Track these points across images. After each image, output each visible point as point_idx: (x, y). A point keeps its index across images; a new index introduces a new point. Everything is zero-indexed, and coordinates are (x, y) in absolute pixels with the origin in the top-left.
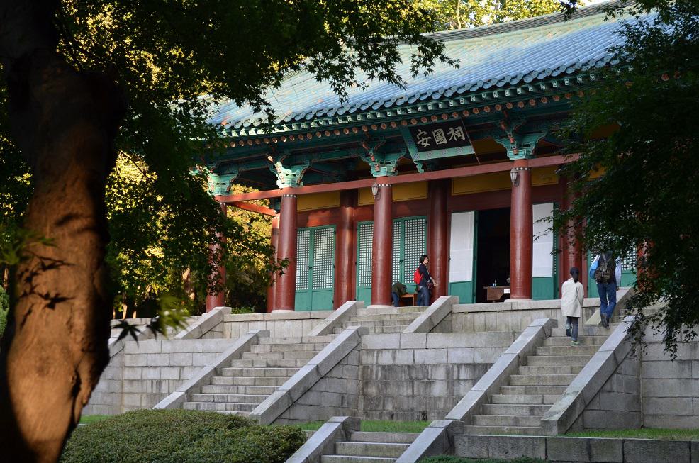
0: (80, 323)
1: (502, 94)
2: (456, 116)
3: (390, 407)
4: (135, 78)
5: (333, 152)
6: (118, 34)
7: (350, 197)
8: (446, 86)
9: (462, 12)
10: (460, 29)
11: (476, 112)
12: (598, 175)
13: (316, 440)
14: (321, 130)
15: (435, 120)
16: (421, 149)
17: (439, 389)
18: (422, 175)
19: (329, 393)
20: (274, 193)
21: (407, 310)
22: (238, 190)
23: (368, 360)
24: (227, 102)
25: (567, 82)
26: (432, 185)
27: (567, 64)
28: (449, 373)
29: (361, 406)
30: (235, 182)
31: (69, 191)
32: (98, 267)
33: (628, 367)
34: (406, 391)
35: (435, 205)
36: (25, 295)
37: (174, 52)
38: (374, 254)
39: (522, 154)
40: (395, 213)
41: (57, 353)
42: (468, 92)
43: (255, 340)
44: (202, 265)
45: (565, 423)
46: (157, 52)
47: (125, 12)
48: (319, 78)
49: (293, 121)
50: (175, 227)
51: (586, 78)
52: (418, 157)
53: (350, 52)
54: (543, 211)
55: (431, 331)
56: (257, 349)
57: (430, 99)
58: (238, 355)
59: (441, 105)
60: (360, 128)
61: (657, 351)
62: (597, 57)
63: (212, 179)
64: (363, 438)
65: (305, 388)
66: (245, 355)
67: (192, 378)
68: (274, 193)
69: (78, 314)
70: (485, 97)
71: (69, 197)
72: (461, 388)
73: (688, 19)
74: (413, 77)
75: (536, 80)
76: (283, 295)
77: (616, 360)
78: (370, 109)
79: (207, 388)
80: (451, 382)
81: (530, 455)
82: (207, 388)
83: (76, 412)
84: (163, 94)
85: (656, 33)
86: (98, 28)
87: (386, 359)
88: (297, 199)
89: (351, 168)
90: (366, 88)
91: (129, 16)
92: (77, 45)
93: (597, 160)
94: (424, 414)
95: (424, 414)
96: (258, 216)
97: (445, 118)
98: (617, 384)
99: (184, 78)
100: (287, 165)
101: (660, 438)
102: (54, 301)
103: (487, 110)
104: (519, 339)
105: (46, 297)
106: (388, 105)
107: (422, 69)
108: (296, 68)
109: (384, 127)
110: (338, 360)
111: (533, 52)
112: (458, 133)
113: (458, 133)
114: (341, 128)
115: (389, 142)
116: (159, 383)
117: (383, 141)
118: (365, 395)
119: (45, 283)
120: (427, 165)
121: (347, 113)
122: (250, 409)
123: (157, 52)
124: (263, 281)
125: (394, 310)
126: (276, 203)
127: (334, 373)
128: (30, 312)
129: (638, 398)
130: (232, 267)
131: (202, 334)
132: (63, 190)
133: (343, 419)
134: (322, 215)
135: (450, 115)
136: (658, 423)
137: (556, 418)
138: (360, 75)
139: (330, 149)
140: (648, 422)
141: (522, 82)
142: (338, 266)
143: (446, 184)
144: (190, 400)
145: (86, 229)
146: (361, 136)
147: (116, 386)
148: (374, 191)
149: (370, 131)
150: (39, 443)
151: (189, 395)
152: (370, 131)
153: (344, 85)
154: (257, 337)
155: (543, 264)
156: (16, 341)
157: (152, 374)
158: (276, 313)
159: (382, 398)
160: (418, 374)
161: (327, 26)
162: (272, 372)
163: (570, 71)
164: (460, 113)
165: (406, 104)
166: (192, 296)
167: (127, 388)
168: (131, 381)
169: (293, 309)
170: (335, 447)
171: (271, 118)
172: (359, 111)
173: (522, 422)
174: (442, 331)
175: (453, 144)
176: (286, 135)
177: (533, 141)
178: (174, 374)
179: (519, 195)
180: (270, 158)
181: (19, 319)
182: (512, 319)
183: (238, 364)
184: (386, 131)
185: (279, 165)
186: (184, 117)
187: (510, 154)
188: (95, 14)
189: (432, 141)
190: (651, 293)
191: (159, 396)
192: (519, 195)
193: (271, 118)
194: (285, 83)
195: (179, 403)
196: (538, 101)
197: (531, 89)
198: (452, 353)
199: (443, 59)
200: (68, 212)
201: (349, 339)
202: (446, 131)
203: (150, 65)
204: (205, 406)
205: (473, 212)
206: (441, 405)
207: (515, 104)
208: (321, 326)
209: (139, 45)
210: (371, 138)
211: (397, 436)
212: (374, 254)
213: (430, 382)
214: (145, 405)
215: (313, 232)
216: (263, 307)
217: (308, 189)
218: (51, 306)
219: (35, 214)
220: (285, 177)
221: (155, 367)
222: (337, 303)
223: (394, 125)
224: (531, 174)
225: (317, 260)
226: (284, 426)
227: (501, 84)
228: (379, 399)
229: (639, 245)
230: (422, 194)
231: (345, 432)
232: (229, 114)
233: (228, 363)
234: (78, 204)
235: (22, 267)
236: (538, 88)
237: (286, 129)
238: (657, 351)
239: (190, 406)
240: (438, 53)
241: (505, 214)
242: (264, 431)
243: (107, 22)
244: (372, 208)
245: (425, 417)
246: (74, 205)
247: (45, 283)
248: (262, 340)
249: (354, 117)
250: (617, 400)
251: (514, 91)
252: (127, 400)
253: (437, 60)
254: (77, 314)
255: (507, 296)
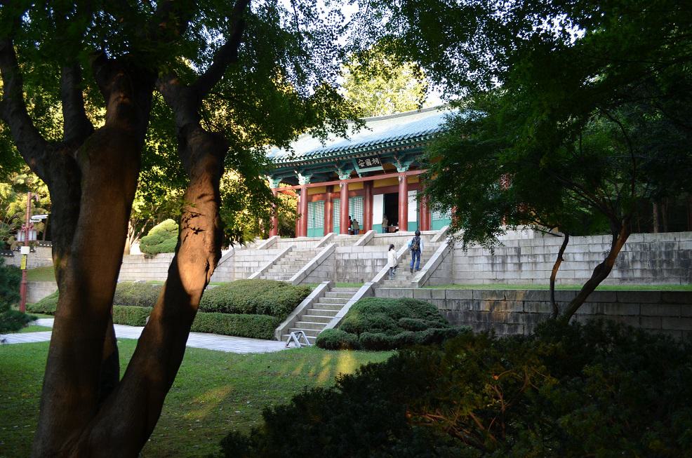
0: (209, 240)
1: (395, 144)
2: (375, 154)
3: (348, 277)
4: (235, 137)
5: (323, 171)
6: (228, 119)
7: (331, 188)
8: (371, 140)
9: (378, 109)
10: (377, 116)
11: (384, 152)
12: (435, 177)
13: (316, 292)
14: (318, 160)
15: (366, 155)
16: (360, 168)
17: (368, 270)
18: (361, 179)
19: (322, 272)
20: (298, 187)
21: (355, 236)
22: (283, 185)
23: (339, 257)
24: (274, 148)
25: (422, 139)
26: (365, 183)
27: (423, 131)
28: (373, 263)
29: (336, 277)
30: (281, 182)
31: (203, 183)
32: (216, 216)
33: (447, 259)
34: (355, 270)
35: (368, 190)
36: (185, 228)
37: (252, 126)
38: (341, 212)
39: (345, 177)
40: (349, 196)
41: (199, 253)
42: (380, 143)
43: (290, 250)
44: (267, 218)
45: (421, 283)
46: (245, 126)
47: (231, 109)
48: (313, 137)
49: (306, 156)
50: (254, 201)
51: (430, 137)
52: (359, 171)
53: (328, 126)
54: (413, 193)
55: (365, 245)
56: (291, 253)
57: (364, 146)
58: (283, 256)
59: (369, 149)
60: (334, 159)
61: (459, 253)
62: (435, 128)
63: (271, 181)
64: (336, 290)
65: (312, 270)
66: (286, 256)
67: (264, 266)
68: (298, 187)
69: (208, 236)
70: (387, 145)
71: (203, 186)
72: (378, 269)
73: (472, 112)
74: (357, 137)
75: (409, 138)
76: (302, 230)
77: (443, 257)
78: (339, 150)
79: (270, 270)
80: (374, 266)
81: (406, 297)
82: (270, 270)
83: (208, 278)
84: (248, 145)
85: (459, 118)
86: (220, 116)
87: (346, 257)
88: (308, 189)
89: (331, 176)
90: (334, 142)
91: (233, 110)
92: (210, 123)
93: (434, 171)
94: (362, 280)
95: (362, 280)
96: (290, 197)
97: (371, 154)
98: (443, 266)
99: (257, 137)
100: (303, 174)
101: (461, 288)
102: (197, 231)
103: (389, 151)
104: (402, 248)
105: (194, 229)
106: (347, 149)
107: (356, 131)
108: (304, 132)
109: (345, 158)
110: (326, 258)
111: (408, 126)
112: (376, 161)
113: (376, 161)
114: (326, 159)
115: (347, 165)
116: (250, 268)
117: (344, 164)
118: (337, 273)
119: (193, 223)
120: (363, 175)
121: (329, 152)
122: (289, 278)
123: (245, 126)
124: (293, 224)
125: (350, 236)
126: (299, 191)
127: (324, 263)
128: (187, 236)
129: (452, 273)
130: (279, 219)
131: (267, 247)
132: (201, 183)
133: (327, 282)
134: (318, 196)
135: (373, 153)
136: (459, 283)
137: (418, 281)
138: (331, 135)
139: (321, 168)
140: (455, 282)
141: (403, 139)
142: (325, 218)
143: (371, 182)
144: (263, 275)
145: (211, 200)
146: (335, 162)
147: (232, 269)
148: (341, 186)
149: (339, 160)
150: (192, 291)
151: (263, 273)
152: (339, 160)
153: (325, 140)
154: (291, 248)
155: (413, 216)
156: (181, 248)
157: (247, 265)
158: (299, 238)
159: (345, 274)
160: (359, 263)
161: (318, 115)
162: (297, 264)
163: (423, 134)
164: (377, 152)
165: (354, 148)
166: (263, 231)
167: (236, 271)
168: (238, 267)
169: (407, 230)
170: (324, 294)
171: (293, 154)
172: (334, 151)
173: (403, 283)
174: (370, 245)
175: (374, 165)
176: (303, 162)
177: (408, 164)
178: (256, 264)
179: (402, 187)
180: (296, 172)
181: (183, 239)
182: (399, 240)
183: (283, 260)
184: (345, 160)
185: (300, 175)
186: (257, 154)
187: (398, 169)
188: (219, 110)
189: (365, 164)
190: (457, 228)
191: (250, 274)
192: (402, 187)
193: (293, 154)
194: (299, 141)
195: (258, 276)
196: (410, 147)
197: (407, 142)
198: (374, 254)
199: (365, 128)
200: (202, 193)
201: (330, 249)
202: (371, 160)
203: (241, 132)
204: (269, 278)
205: (383, 195)
206: (369, 276)
207: (400, 148)
208: (319, 243)
209: (237, 123)
210: (339, 163)
211: (351, 289)
212: (341, 212)
213: (365, 267)
214: (244, 277)
215: (315, 203)
216: (294, 236)
217: (312, 185)
218: (196, 233)
219: (188, 194)
220: (303, 180)
221: (560, 259)
222: (325, 234)
223: (349, 158)
224: (407, 178)
225: (317, 215)
226: (303, 286)
227: (394, 140)
228: (343, 274)
229: (453, 207)
230: (362, 187)
231: (329, 288)
232: (274, 152)
233: (279, 259)
234: (207, 189)
235: (183, 217)
236: (410, 141)
237: (302, 159)
238: (459, 253)
239: (263, 278)
240: (364, 125)
241: (396, 195)
242: (294, 288)
243: (224, 113)
244: (340, 193)
245: (362, 281)
246: (205, 190)
247: (193, 223)
248: (293, 249)
249: (332, 154)
250: (443, 273)
251: (400, 143)
252: (236, 276)
253: (362, 128)
254: (207, 236)
255: (397, 230)
